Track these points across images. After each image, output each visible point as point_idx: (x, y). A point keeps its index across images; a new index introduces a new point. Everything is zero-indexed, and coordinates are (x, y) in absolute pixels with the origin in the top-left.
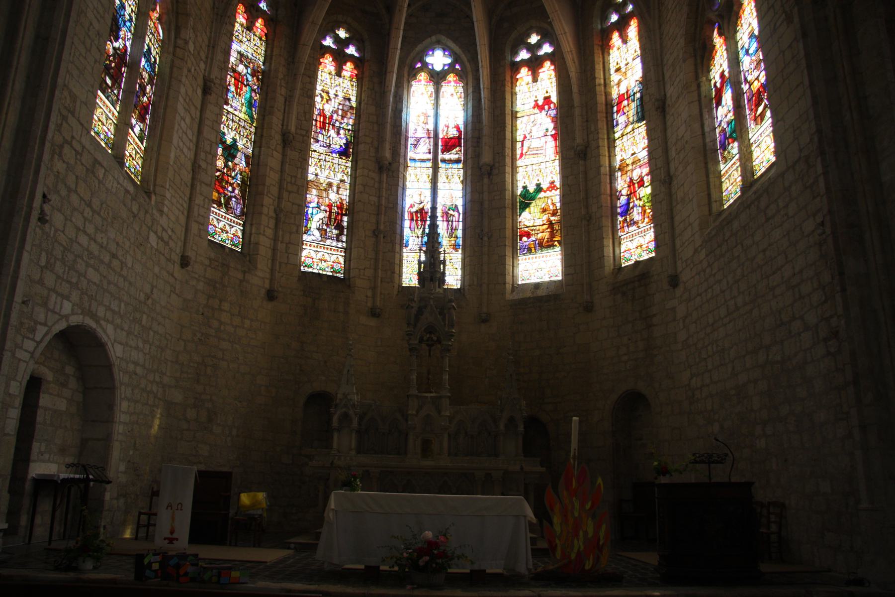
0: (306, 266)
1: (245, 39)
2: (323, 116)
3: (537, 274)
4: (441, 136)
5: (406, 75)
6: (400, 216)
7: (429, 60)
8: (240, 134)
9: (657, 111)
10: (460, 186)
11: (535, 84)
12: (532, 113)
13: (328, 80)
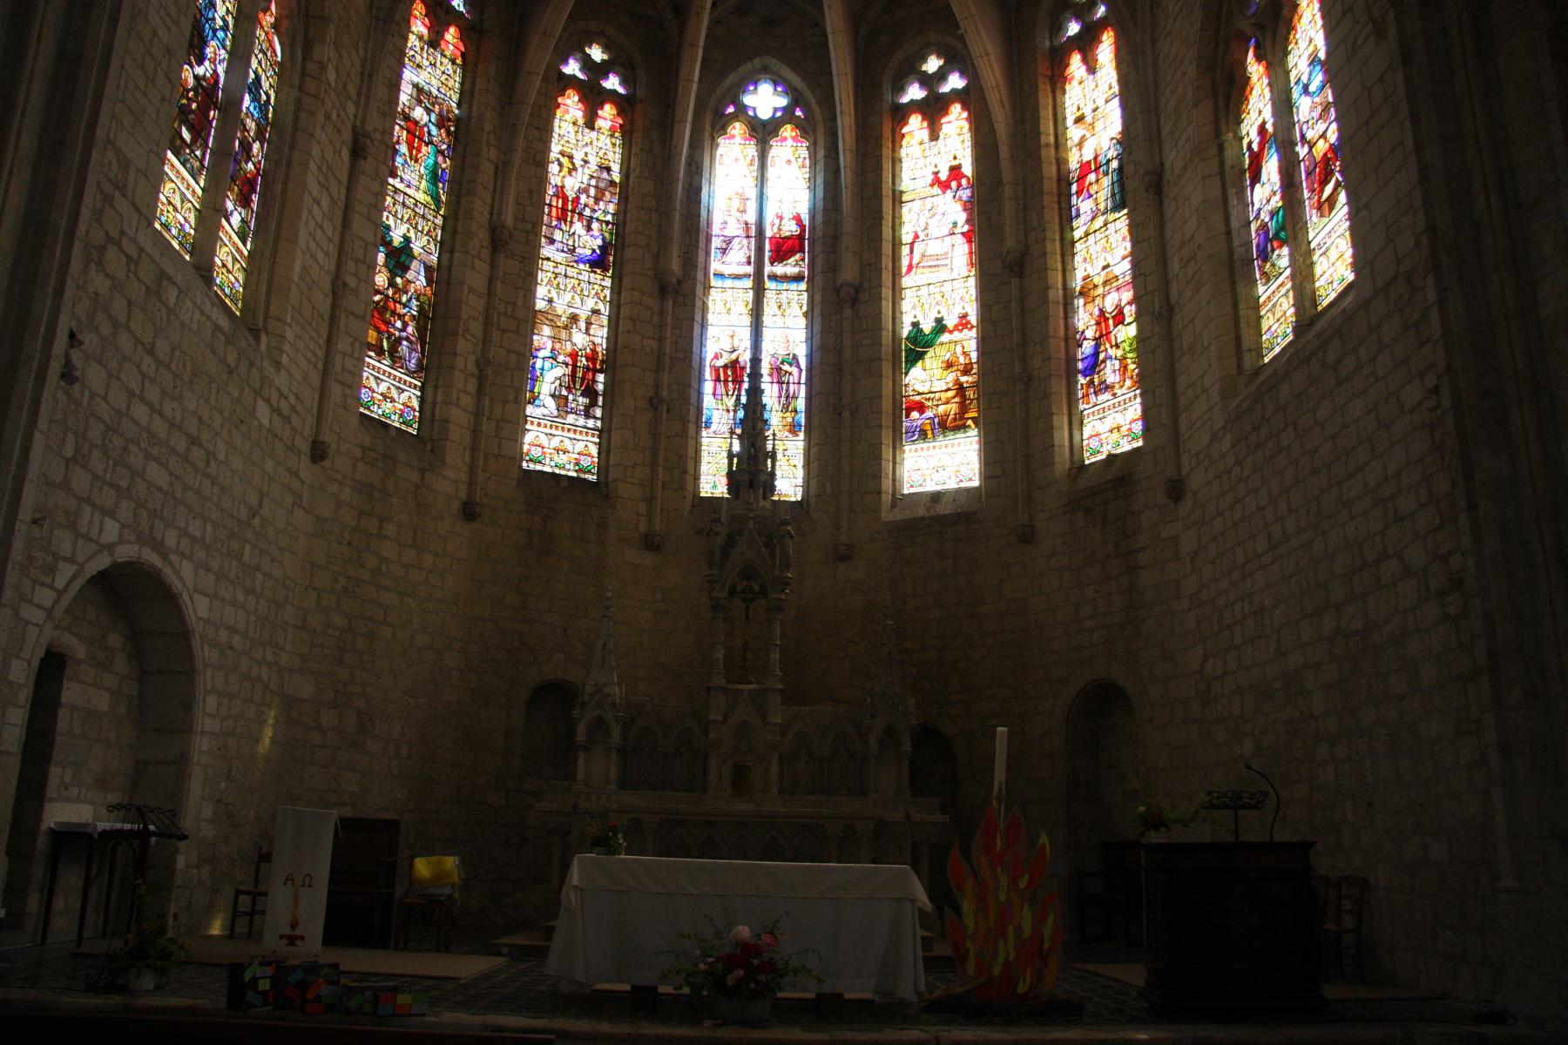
0: (531, 460)
1: (426, 63)
4: (769, 234)
5: (708, 127)
6: (697, 373)
7: (748, 100)
8: (416, 228)
10: (802, 322)
11: (934, 143)
12: (929, 194)
13: (572, 135)
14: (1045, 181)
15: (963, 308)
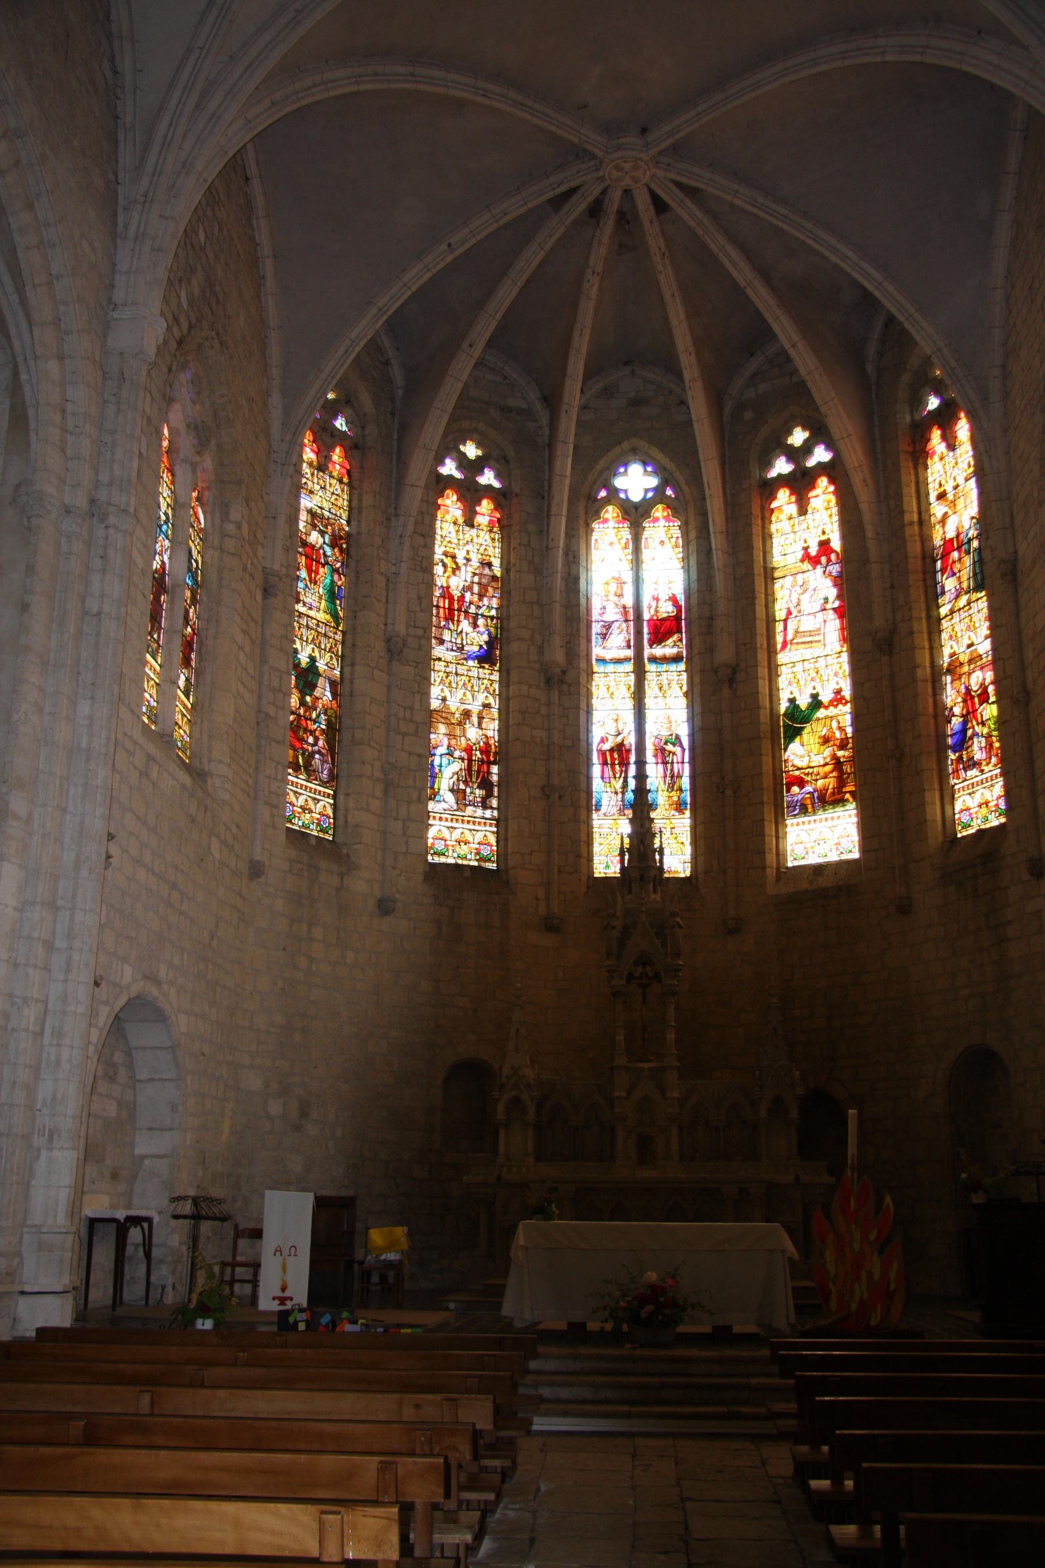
0: (435, 853)
1: (317, 487)
2: (449, 598)
3: (817, 849)
4: (646, 616)
5: (582, 514)
6: (585, 759)
7: (619, 482)
8: (319, 647)
9: (1002, 579)
10: (683, 702)
11: (803, 518)
12: (799, 569)
13: (453, 535)
14: (910, 560)
15: (838, 684)
